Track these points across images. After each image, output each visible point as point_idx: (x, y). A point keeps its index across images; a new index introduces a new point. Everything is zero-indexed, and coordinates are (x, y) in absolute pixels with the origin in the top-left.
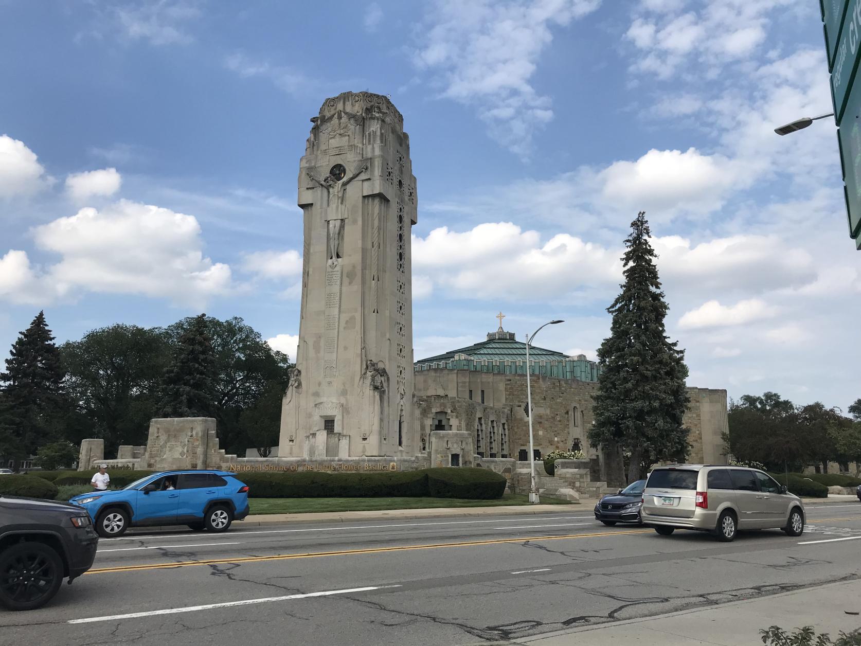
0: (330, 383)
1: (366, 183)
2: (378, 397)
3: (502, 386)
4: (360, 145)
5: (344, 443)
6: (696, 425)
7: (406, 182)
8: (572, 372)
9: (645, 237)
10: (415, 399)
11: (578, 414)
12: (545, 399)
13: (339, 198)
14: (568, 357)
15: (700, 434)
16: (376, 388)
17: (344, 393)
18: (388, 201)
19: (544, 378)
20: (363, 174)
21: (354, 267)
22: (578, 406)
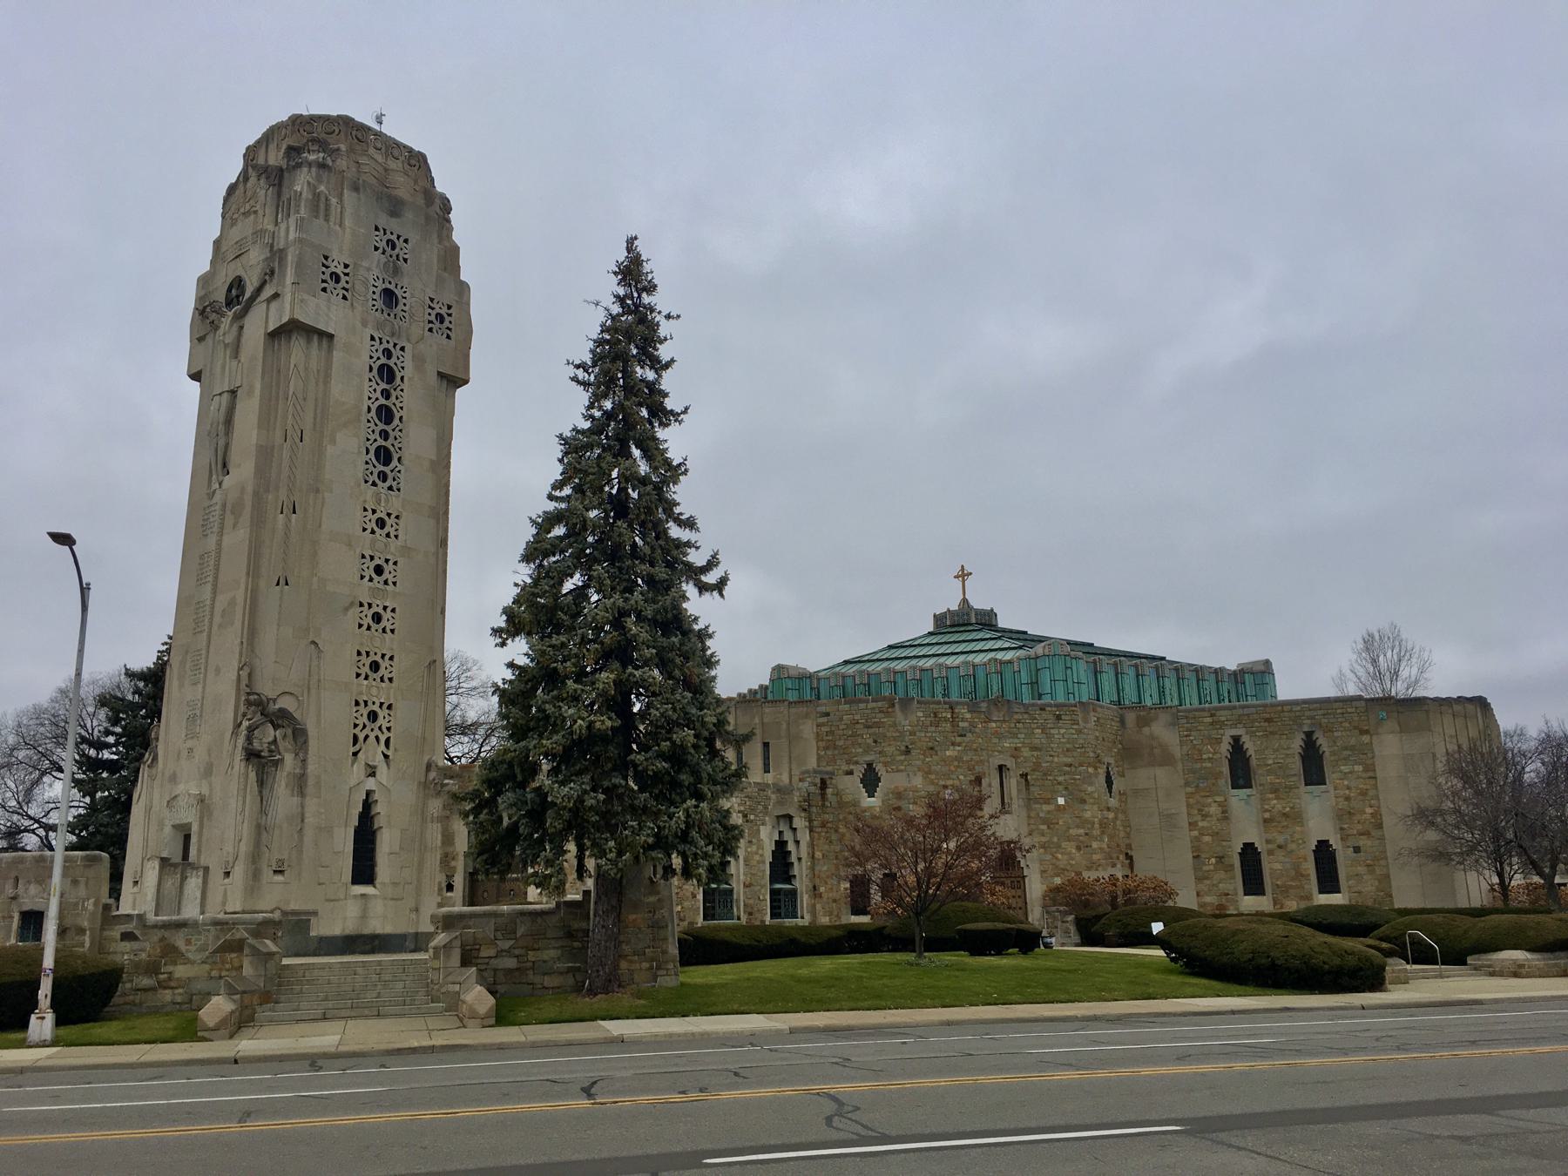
0: (190, 750)
1: (274, 305)
2: (253, 775)
3: (808, 729)
4: (271, 227)
5: (193, 883)
6: (1364, 793)
7: (416, 289)
8: (1034, 683)
9: (646, 299)
10: (432, 775)
11: (1013, 783)
12: (907, 751)
13: (226, 346)
14: (1040, 640)
15: (1377, 815)
16: (251, 755)
17: (208, 771)
18: (331, 337)
19: (906, 702)
20: (267, 286)
21: (243, 490)
22: (1010, 763)
